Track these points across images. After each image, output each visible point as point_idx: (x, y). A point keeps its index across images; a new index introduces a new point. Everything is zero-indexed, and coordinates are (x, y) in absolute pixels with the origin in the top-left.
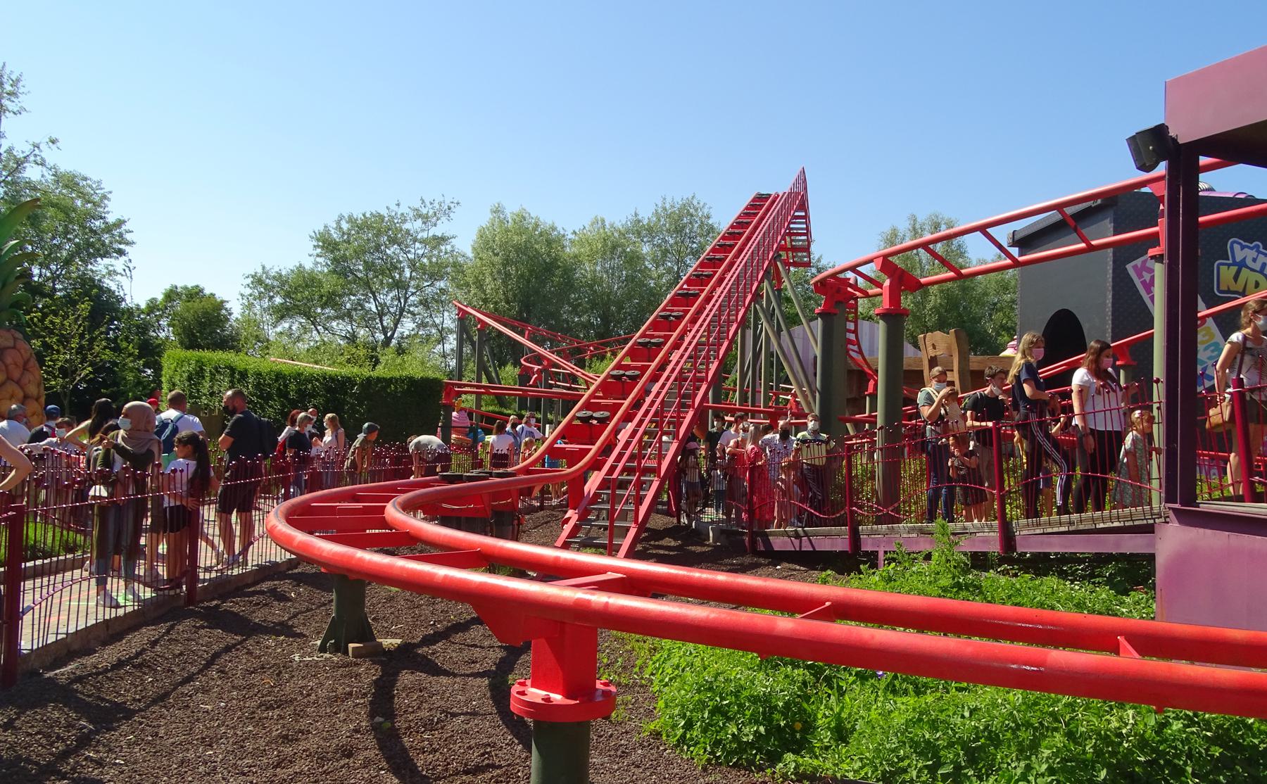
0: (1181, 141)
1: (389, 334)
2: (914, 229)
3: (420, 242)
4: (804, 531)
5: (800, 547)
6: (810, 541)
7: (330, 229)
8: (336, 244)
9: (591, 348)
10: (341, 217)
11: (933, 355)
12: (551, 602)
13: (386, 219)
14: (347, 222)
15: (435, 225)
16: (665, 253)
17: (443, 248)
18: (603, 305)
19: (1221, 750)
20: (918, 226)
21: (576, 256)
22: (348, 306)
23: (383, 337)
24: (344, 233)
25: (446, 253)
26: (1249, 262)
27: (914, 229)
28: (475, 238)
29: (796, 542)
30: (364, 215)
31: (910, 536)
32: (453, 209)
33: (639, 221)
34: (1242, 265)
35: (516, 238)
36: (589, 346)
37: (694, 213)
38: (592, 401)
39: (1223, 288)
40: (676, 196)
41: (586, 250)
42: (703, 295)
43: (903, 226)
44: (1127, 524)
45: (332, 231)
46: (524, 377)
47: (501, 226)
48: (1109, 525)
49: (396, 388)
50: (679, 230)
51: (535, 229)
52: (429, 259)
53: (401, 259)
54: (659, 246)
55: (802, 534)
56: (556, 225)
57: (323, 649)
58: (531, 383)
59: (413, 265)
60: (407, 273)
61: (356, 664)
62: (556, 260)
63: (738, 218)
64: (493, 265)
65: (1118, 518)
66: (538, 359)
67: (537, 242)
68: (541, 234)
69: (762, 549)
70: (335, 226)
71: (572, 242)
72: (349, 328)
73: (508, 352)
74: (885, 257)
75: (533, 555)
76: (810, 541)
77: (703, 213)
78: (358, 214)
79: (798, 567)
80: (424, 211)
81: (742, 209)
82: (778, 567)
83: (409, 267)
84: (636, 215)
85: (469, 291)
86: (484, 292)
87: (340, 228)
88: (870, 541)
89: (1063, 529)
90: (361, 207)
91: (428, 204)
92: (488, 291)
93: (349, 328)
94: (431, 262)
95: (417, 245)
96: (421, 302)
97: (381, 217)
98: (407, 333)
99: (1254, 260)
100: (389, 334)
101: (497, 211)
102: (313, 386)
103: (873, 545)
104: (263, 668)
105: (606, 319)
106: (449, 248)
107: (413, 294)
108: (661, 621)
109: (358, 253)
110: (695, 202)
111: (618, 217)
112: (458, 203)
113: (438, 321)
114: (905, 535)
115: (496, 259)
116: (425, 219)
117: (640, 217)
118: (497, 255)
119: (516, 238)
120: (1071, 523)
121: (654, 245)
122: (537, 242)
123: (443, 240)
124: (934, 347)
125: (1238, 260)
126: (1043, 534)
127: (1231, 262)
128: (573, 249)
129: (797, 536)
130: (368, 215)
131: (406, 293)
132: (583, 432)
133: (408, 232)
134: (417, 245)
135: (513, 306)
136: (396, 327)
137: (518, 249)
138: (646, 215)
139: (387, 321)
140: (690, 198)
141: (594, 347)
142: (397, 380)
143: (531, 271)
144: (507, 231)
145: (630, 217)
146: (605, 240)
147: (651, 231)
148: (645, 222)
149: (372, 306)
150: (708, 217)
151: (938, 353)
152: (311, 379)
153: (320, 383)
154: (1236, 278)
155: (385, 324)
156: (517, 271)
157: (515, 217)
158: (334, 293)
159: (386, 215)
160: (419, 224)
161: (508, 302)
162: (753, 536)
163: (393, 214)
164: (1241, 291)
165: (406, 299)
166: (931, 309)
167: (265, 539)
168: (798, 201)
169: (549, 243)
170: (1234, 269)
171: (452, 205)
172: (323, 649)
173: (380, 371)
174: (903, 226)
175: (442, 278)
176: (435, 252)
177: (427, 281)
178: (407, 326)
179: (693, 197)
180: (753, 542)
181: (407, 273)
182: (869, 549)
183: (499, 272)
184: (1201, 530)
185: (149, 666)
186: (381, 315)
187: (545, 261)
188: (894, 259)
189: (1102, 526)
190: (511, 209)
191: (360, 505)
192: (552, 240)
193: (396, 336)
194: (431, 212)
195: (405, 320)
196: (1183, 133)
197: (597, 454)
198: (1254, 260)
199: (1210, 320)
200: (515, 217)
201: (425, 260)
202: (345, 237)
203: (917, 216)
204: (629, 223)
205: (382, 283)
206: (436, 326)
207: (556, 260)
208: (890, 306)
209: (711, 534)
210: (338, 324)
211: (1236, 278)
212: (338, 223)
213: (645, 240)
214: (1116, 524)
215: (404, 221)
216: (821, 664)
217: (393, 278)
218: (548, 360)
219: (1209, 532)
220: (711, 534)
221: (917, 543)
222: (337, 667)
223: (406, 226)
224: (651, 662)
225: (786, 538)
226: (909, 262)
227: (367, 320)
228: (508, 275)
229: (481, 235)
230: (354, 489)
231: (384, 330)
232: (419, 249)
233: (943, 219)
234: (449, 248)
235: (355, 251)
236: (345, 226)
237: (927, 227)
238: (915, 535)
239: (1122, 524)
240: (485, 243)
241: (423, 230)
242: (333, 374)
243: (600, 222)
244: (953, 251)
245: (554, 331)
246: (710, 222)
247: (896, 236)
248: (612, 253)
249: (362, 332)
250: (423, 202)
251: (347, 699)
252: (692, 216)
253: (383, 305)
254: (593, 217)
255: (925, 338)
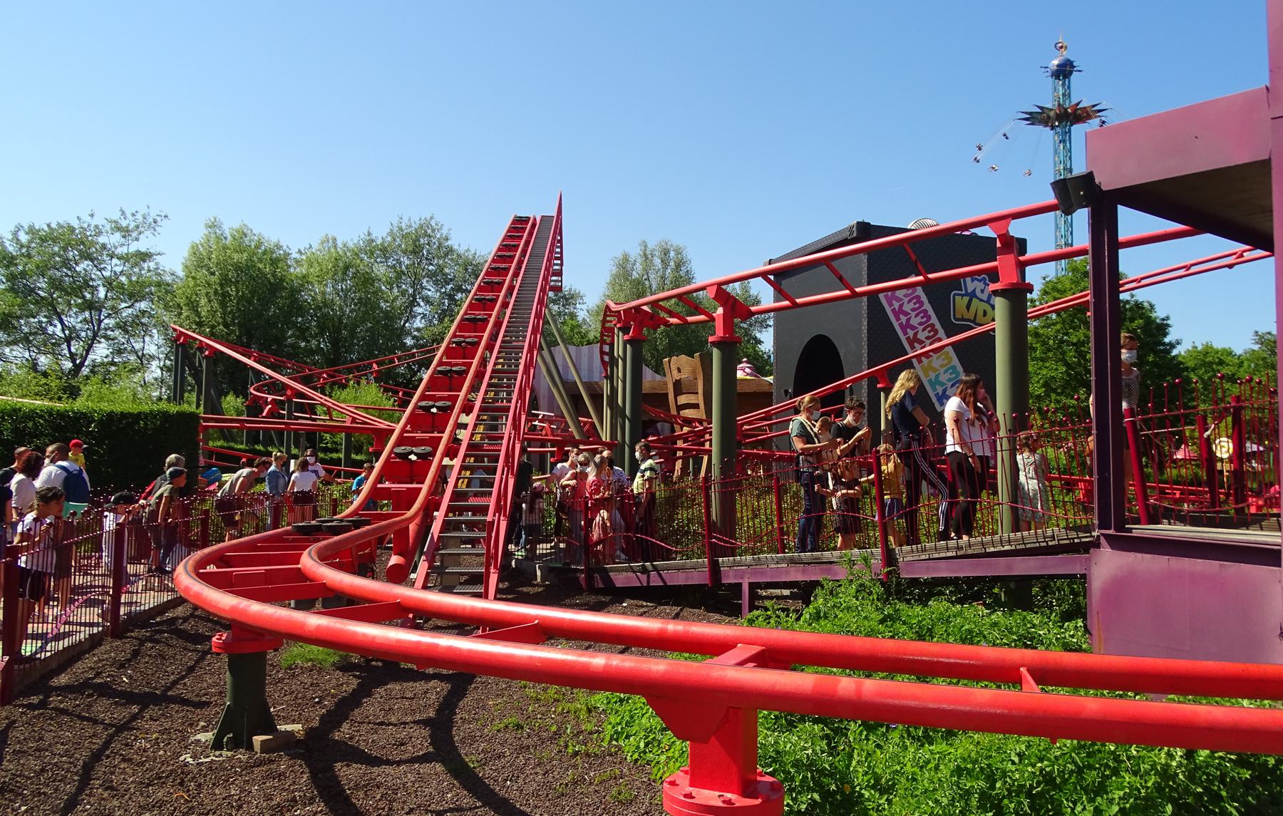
0: (1104, 188)
1: (78, 362)
2: (645, 255)
3: (118, 258)
4: (653, 566)
5: (648, 582)
6: (660, 576)
7: (5, 240)
8: (13, 258)
9: (325, 375)
10: (19, 228)
11: (678, 378)
12: (778, 691)
13: (77, 231)
14: (27, 233)
15: (137, 239)
16: (400, 274)
17: (145, 266)
18: (330, 325)
19: (1250, 772)
20: (648, 252)
21: (304, 277)
22: (26, 330)
23: (71, 364)
24: (22, 246)
25: (149, 271)
26: (978, 293)
27: (645, 255)
28: (186, 254)
29: (643, 578)
30: (49, 226)
31: (779, 566)
32: (160, 223)
33: (373, 241)
34: (973, 295)
35: (236, 256)
36: (323, 373)
37: (431, 234)
38: (405, 435)
39: (958, 316)
40: (413, 216)
41: (315, 270)
42: (492, 320)
43: (635, 252)
44: (1018, 547)
45: (7, 244)
46: (255, 407)
47: (218, 243)
48: (1000, 548)
49: (146, 424)
50: (416, 250)
51: (257, 247)
52: (129, 277)
53: (93, 276)
54: (394, 267)
55: (650, 568)
56: (281, 244)
57: (217, 745)
58: (264, 414)
59: (109, 283)
60: (102, 293)
61: (271, 761)
62: (282, 280)
63: (503, 241)
64: (209, 284)
65: (1009, 541)
66: (275, 387)
67: (260, 260)
68: (265, 253)
69: (601, 585)
70: (10, 237)
71: (297, 261)
72: (27, 355)
73: (237, 378)
74: (720, 284)
75: (596, 624)
76: (660, 576)
77: (442, 235)
78: (41, 224)
79: (644, 604)
80: (124, 223)
81: (504, 232)
82: (625, 605)
83: (104, 285)
84: (369, 234)
85: (181, 314)
86: (198, 315)
87: (18, 240)
88: (731, 573)
89: (950, 554)
90: (47, 216)
91: (129, 216)
92: (203, 314)
93: (27, 355)
94: (130, 281)
95: (115, 261)
96: (118, 326)
97: (72, 230)
98: (99, 360)
99: (982, 291)
100: (78, 362)
101: (213, 225)
102: (35, 424)
103: (735, 577)
104: (160, 778)
105: (335, 342)
106: (152, 265)
107: (109, 316)
108: (921, 709)
109: (42, 270)
110: (433, 223)
111: (350, 236)
112: (166, 216)
113: (138, 346)
114: (773, 566)
115: (214, 279)
116: (125, 232)
117: (373, 237)
118: (213, 274)
119: (236, 256)
120: (959, 548)
121: (388, 266)
122: (260, 260)
123: (145, 256)
124: (679, 370)
125: (969, 291)
126: (929, 559)
127: (964, 292)
128: (298, 270)
129: (644, 570)
130: (54, 226)
131: (100, 316)
132: (403, 469)
133: (104, 246)
134: (115, 261)
135: (233, 330)
136: (87, 354)
137: (238, 267)
138: (381, 234)
139: (76, 347)
140: (428, 218)
141: (328, 375)
142: (146, 415)
143: (253, 292)
144: (225, 248)
145: (362, 236)
146: (336, 259)
147: (385, 251)
148: (379, 241)
149: (58, 330)
150: (447, 239)
151: (683, 377)
152: (32, 415)
153: (45, 420)
154: (968, 307)
155: (73, 350)
156: (237, 291)
157: (235, 233)
158: (10, 315)
159: (77, 227)
160: (117, 238)
161: (226, 326)
162: (589, 572)
163: (85, 225)
164: (972, 318)
165: (100, 321)
166: (662, 333)
167: (84, 609)
168: (553, 227)
169: (274, 262)
170: (966, 299)
171: (158, 219)
172: (217, 745)
173: (80, 404)
174: (635, 252)
175: (143, 298)
176: (136, 270)
177: (126, 302)
178: (101, 351)
179: (431, 218)
180: (590, 579)
181: (102, 293)
182: (733, 581)
183: (216, 292)
184: (1139, 555)
185: (11, 791)
186: (68, 340)
187: (269, 282)
188: (729, 288)
189: (992, 549)
190: (229, 225)
191: (262, 569)
192: (277, 260)
193: (86, 363)
194: (132, 225)
195: (97, 345)
196: (1107, 181)
197: (430, 493)
198: (982, 291)
199: (950, 349)
200: (235, 233)
201: (123, 279)
202: (24, 250)
203: (648, 242)
204: (361, 242)
205: (69, 304)
206: (135, 352)
207: (282, 280)
208: (725, 333)
209: (539, 573)
210: (12, 350)
211: (968, 307)
212: (15, 234)
213: (378, 260)
214: (1007, 548)
215: (99, 233)
216: (1221, 754)
217: (84, 297)
218: (292, 388)
219: (1148, 556)
220: (539, 573)
221: (787, 573)
222: (248, 767)
223: (102, 240)
224: (610, 727)
225: (630, 574)
226: (640, 287)
227: (52, 346)
228: (225, 295)
229: (195, 251)
230: (221, 550)
231: (72, 357)
232: (116, 266)
233: (672, 245)
234: (152, 265)
235: (38, 267)
236: (24, 238)
237: (657, 253)
238: (784, 565)
239: (1013, 548)
240: (199, 261)
241: (122, 245)
242: (62, 410)
243: (331, 241)
244: (681, 277)
245: (276, 353)
246: (449, 243)
247: (627, 260)
248: (344, 273)
249: (43, 360)
250: (123, 213)
251: (293, 807)
252: (430, 236)
253: (72, 329)
254: (324, 235)
255: (669, 362)
